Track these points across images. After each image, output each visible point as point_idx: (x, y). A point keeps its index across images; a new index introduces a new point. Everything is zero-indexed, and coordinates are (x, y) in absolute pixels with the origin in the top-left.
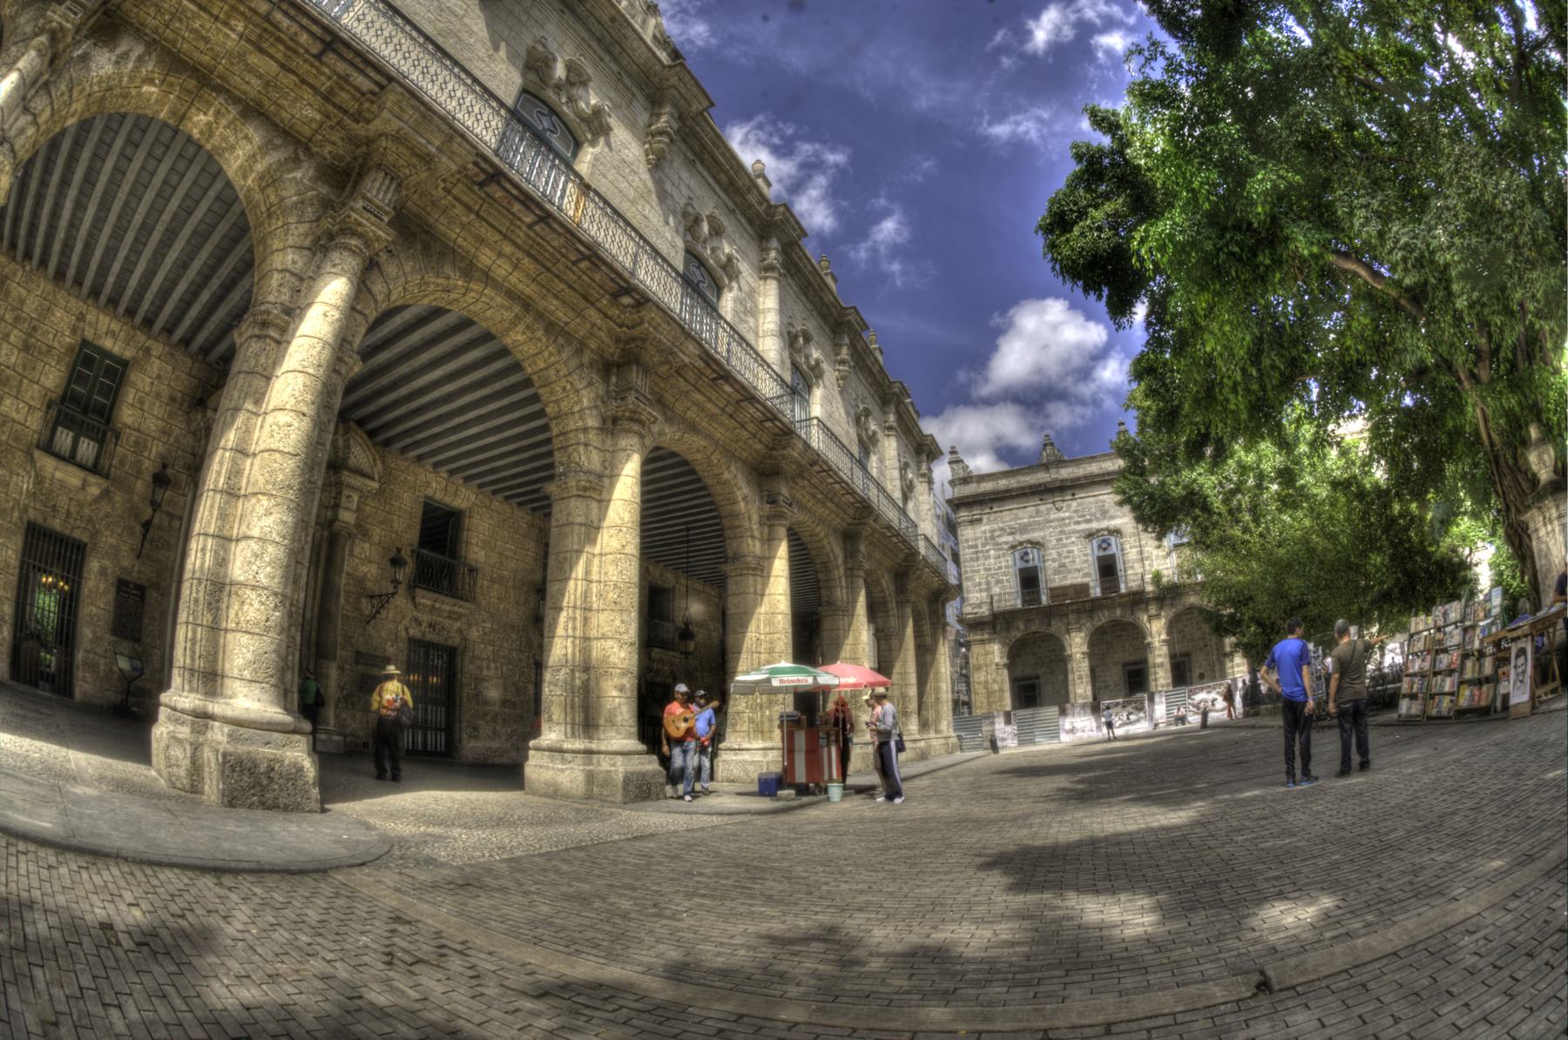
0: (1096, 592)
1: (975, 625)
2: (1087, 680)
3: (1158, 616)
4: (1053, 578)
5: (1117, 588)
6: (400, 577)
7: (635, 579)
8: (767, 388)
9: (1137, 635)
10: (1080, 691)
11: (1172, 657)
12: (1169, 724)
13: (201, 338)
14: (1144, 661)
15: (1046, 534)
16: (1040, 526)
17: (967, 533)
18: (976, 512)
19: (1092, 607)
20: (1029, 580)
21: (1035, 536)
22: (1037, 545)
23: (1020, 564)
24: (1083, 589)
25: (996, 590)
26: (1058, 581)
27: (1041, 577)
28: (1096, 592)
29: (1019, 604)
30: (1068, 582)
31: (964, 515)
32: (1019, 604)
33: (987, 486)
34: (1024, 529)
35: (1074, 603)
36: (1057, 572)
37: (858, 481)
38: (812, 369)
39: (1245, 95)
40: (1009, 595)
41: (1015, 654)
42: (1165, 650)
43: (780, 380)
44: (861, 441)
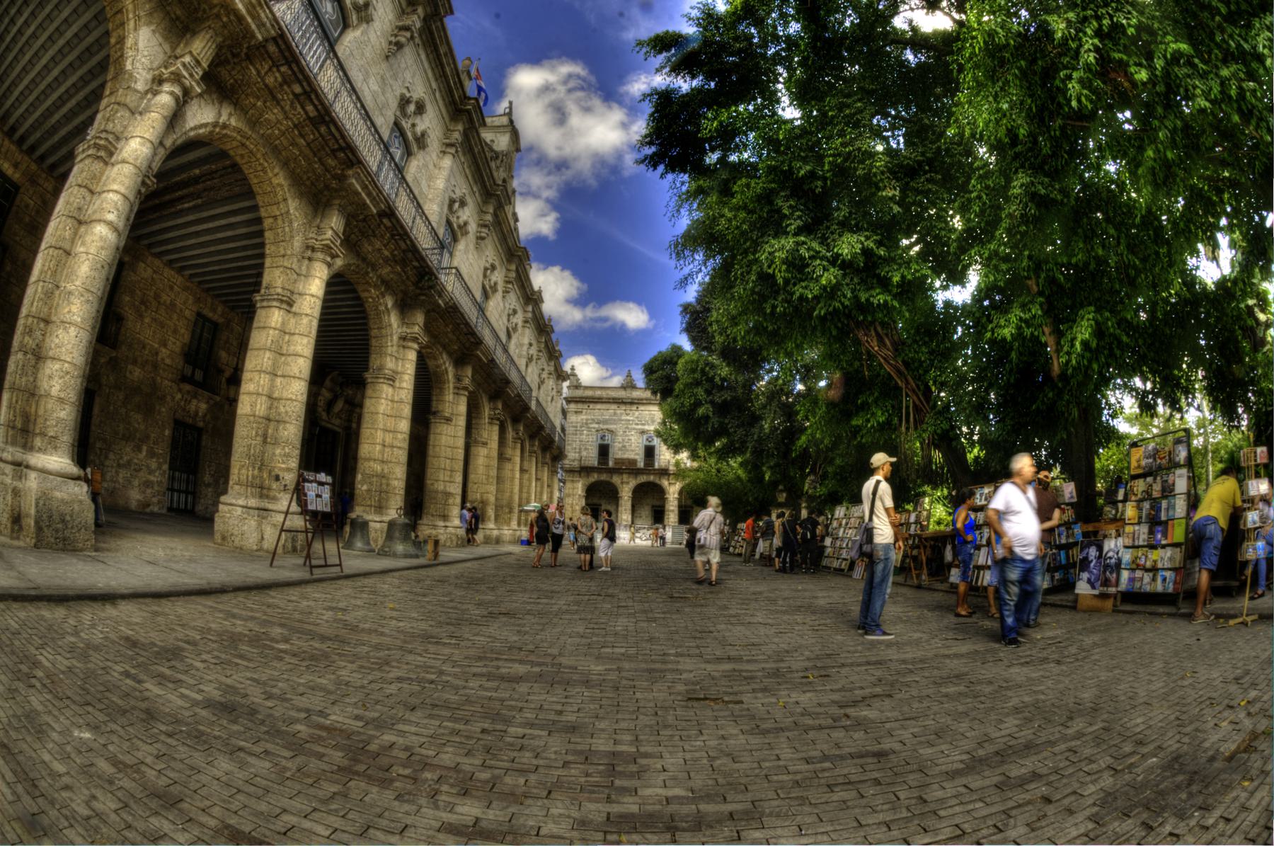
0: (641, 465)
1: (571, 471)
2: (629, 512)
3: (1208, 518)
4: (616, 453)
5: (653, 465)
6: (264, 380)
7: (249, 354)
8: (424, 241)
9: (660, 492)
10: (624, 517)
11: (680, 506)
12: (673, 543)
13: (51, 160)
14: (663, 506)
15: (618, 428)
16: (615, 422)
17: (572, 418)
18: (580, 406)
19: (635, 472)
20: (604, 451)
21: (612, 427)
22: (611, 431)
23: (600, 441)
24: (634, 462)
25: (584, 454)
26: (620, 455)
27: (611, 451)
28: (641, 465)
29: (596, 464)
30: (626, 456)
31: (573, 407)
32: (596, 464)
33: (589, 393)
34: (605, 422)
35: (628, 468)
36: (620, 449)
37: (387, 180)
38: (460, 227)
39: (853, 78)
40: (591, 457)
41: (591, 491)
42: (676, 503)
43: (433, 232)
44: (484, 287)
